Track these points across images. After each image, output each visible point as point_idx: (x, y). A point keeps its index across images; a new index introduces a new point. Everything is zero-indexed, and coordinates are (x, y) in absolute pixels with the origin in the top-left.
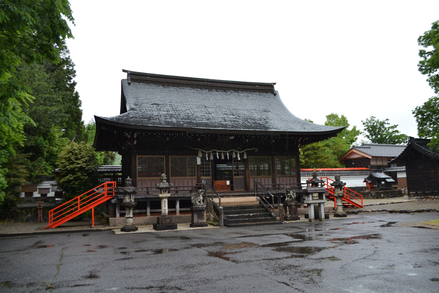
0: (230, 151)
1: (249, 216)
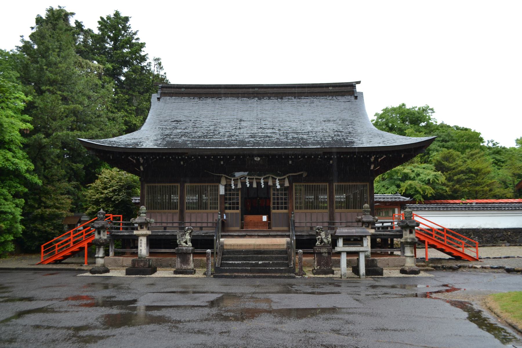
0: (265, 176)
1: (257, 265)
